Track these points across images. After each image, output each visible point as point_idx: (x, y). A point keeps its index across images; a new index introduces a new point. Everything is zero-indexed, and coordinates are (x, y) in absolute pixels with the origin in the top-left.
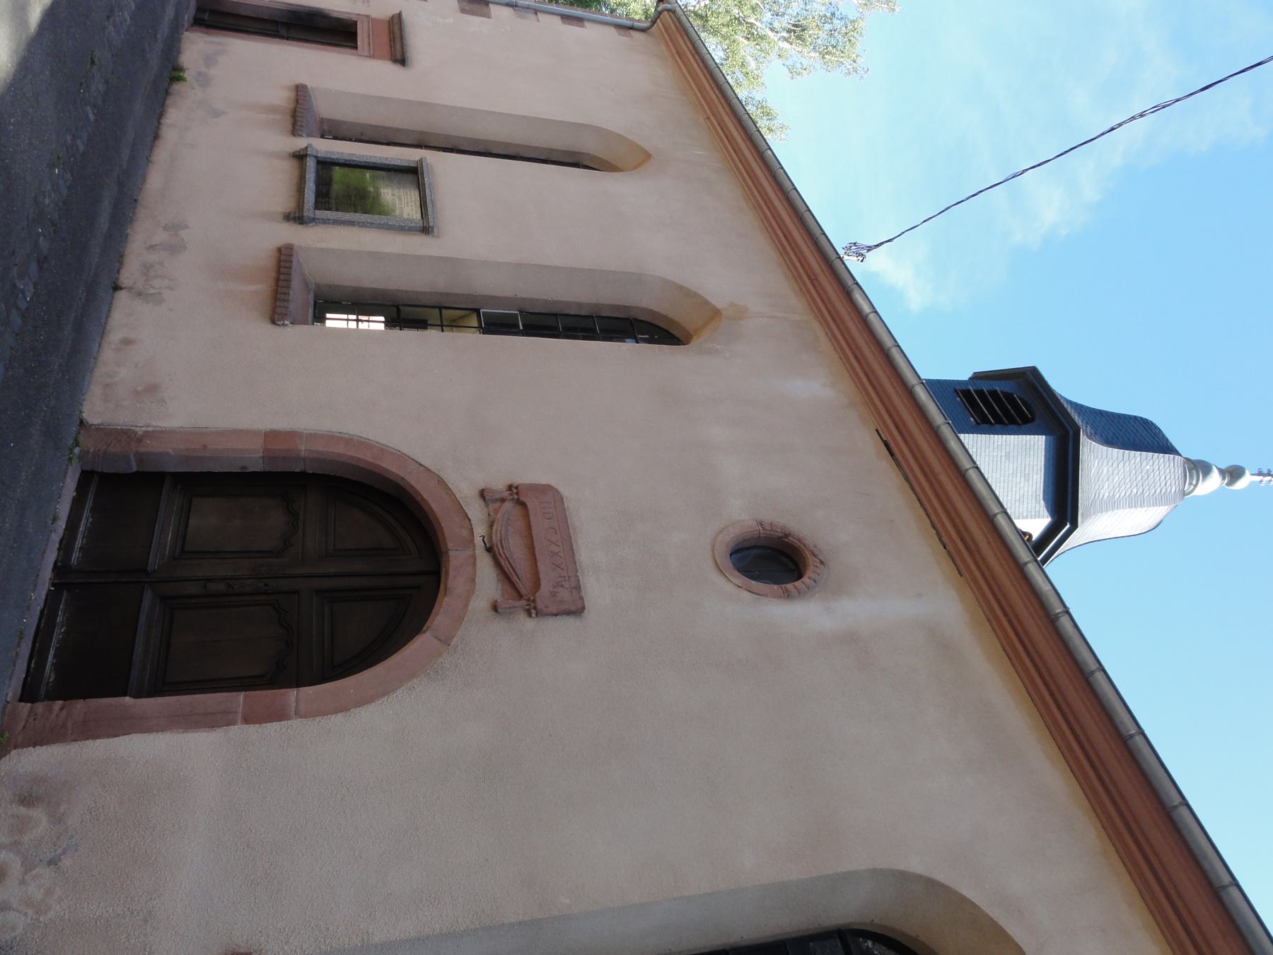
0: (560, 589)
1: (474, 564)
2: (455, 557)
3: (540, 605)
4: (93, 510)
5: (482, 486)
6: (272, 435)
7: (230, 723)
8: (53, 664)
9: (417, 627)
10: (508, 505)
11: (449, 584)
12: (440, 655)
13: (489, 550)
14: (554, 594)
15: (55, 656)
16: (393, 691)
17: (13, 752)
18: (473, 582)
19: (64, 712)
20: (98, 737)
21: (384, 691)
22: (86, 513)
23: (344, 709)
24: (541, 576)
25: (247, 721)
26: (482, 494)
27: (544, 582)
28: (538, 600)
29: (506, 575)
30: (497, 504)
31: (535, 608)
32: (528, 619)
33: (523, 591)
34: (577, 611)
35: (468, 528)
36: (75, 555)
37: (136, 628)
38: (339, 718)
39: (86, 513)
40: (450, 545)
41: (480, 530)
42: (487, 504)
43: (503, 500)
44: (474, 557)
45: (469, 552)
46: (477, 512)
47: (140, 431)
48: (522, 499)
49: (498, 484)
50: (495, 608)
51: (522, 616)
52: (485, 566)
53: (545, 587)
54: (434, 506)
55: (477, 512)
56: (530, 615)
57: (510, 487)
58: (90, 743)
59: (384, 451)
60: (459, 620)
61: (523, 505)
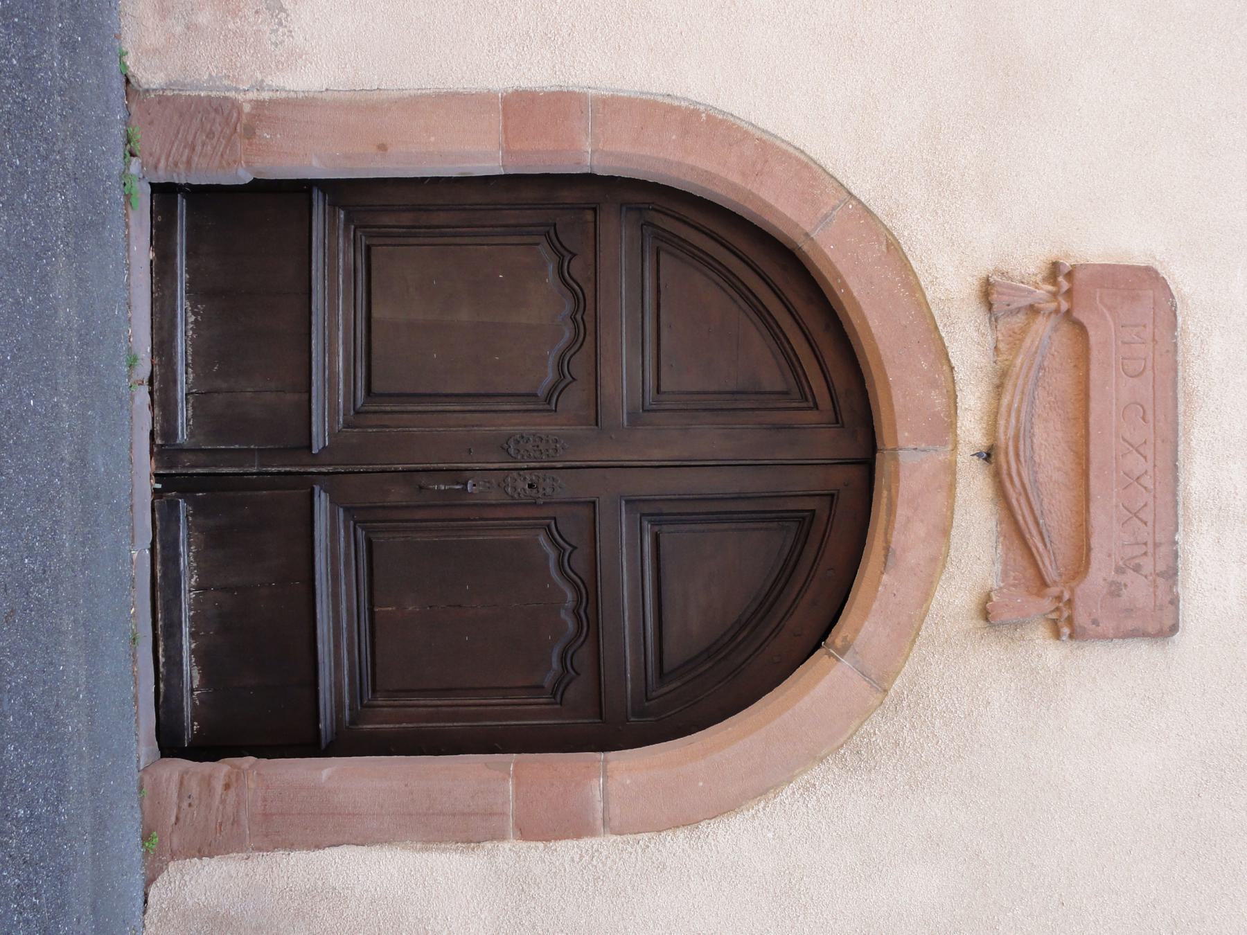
0: (1130, 576)
1: (952, 486)
2: (909, 466)
3: (1082, 619)
4: (191, 253)
5: (985, 266)
6: (521, 107)
7: (501, 837)
8: (193, 652)
9: (819, 634)
10: (1042, 327)
11: (897, 538)
12: (866, 714)
13: (988, 456)
14: (1115, 590)
15: (192, 635)
16: (777, 787)
17: (172, 866)
18: (943, 538)
19: (232, 796)
20: (291, 846)
21: (757, 788)
22: (182, 303)
23: (685, 820)
24: (1095, 541)
25: (525, 834)
26: (987, 292)
27: (1097, 556)
28: (1078, 603)
29: (1016, 529)
30: (1020, 319)
31: (1070, 620)
32: (1051, 642)
33: (1050, 572)
34: (1162, 626)
35: (951, 395)
36: (183, 414)
37: (313, 579)
38: (676, 842)
39: (182, 303)
40: (904, 436)
41: (971, 429)
42: (994, 319)
43: (1033, 310)
44: (951, 469)
45: (942, 456)
46: (969, 345)
47: (246, 98)
48: (1077, 314)
49: (1027, 263)
50: (986, 613)
51: (1039, 635)
52: (973, 489)
53: (1100, 572)
54: (874, 323)
55: (969, 345)
56: (1057, 635)
57: (1054, 271)
58: (279, 855)
59: (768, 151)
60: (908, 633)
61: (1081, 329)
